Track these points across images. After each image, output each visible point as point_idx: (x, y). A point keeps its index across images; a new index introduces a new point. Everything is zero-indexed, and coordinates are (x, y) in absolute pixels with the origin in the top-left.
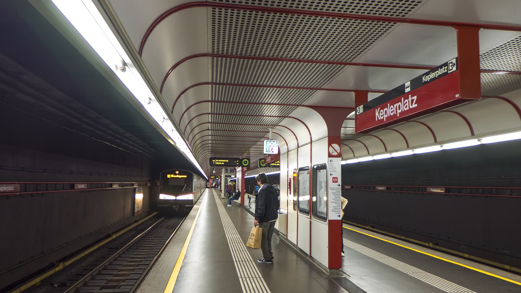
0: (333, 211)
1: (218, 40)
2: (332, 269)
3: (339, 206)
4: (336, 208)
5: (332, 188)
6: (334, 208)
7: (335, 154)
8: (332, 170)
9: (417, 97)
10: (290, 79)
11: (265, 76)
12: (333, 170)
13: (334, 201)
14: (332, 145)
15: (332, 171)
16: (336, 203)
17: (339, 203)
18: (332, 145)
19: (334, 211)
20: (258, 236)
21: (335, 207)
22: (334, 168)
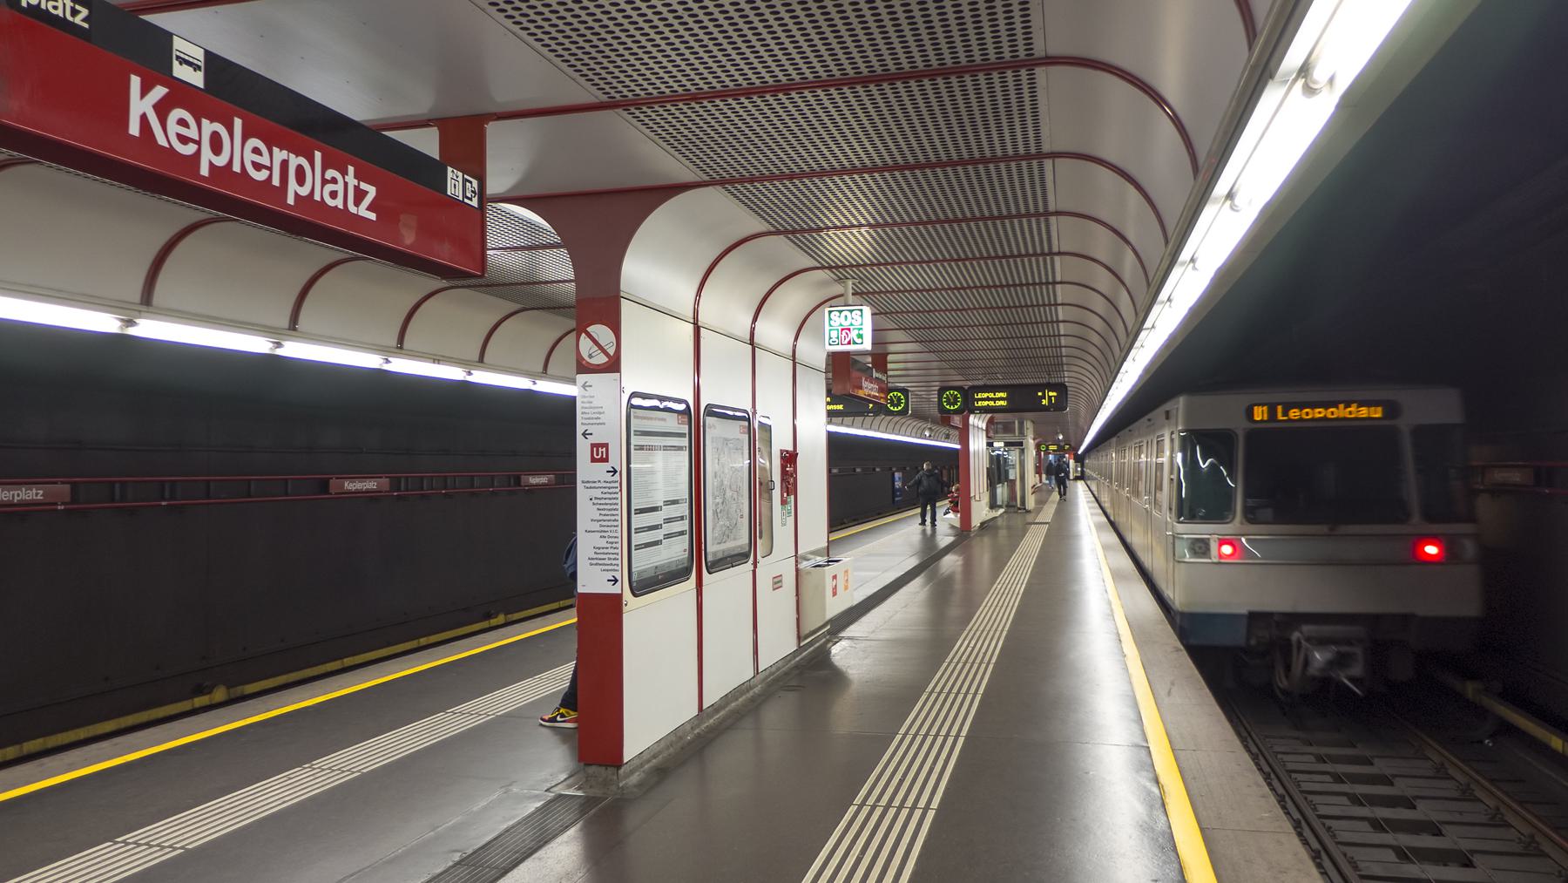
0: (591, 564)
1: (1001, 47)
2: (591, 765)
3: (614, 545)
4: (603, 553)
5: (588, 482)
6: (595, 553)
7: (601, 359)
8: (589, 419)
9: (135, 75)
10: (772, 117)
11: (1000, 98)
12: (592, 418)
13: (596, 526)
14: (589, 329)
15: (591, 421)
16: (603, 534)
17: (611, 534)
18: (589, 329)
19: (596, 564)
20: (1105, 595)
21: (599, 548)
22: (596, 410)
